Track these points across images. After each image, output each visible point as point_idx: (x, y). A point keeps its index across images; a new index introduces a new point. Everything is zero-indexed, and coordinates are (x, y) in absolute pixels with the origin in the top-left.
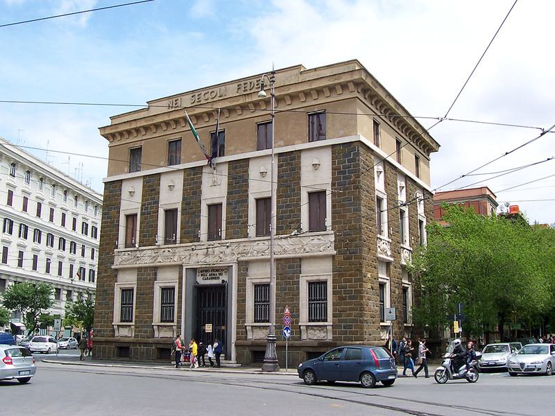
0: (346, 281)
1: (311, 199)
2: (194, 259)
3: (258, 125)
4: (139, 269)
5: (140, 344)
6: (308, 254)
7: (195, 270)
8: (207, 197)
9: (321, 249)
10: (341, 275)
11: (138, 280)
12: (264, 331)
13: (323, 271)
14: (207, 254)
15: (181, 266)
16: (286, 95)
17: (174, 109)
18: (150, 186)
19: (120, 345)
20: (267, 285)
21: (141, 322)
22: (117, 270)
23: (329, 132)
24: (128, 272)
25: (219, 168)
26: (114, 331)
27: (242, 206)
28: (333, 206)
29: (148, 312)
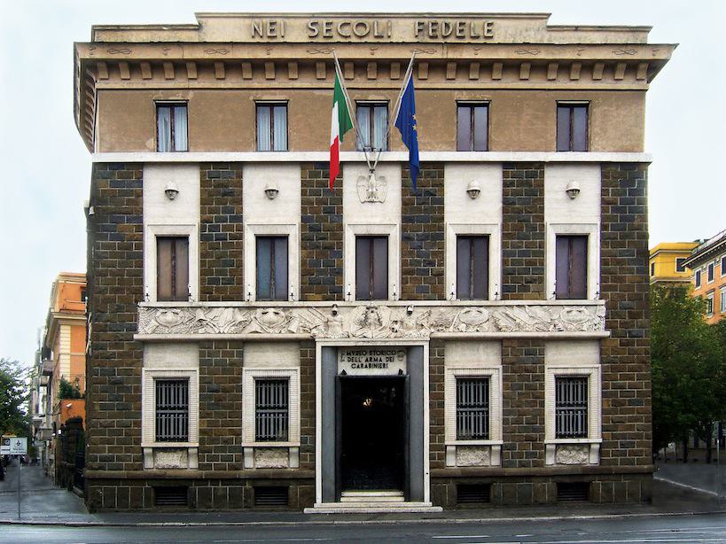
3: (158, 106)
5: (215, 480)
8: (355, 221)
11: (202, 363)
13: (585, 361)
14: (364, 323)
15: (311, 342)
17: (265, 40)
18: (219, 185)
20: (584, 380)
22: (145, 343)
23: (595, 140)
24: (268, 348)
26: (142, 458)
27: (433, 246)
28: (603, 262)
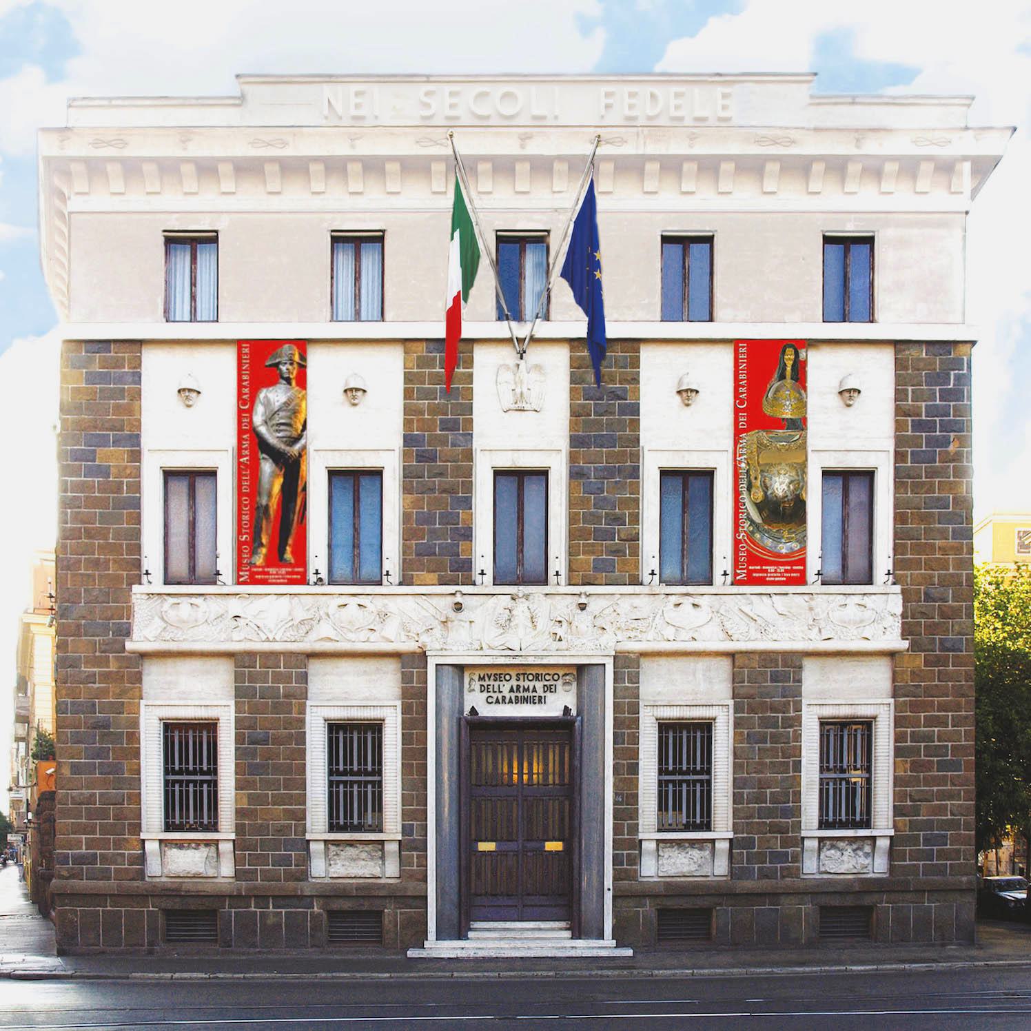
0: (931, 722)
1: (664, 487)
4: (732, 655)
5: (262, 899)
7: (460, 668)
12: (696, 853)
16: (272, 160)
19: (176, 904)
21: (261, 830)
22: (144, 655)
25: (536, 355)
28: (899, 518)
29: (289, 800)
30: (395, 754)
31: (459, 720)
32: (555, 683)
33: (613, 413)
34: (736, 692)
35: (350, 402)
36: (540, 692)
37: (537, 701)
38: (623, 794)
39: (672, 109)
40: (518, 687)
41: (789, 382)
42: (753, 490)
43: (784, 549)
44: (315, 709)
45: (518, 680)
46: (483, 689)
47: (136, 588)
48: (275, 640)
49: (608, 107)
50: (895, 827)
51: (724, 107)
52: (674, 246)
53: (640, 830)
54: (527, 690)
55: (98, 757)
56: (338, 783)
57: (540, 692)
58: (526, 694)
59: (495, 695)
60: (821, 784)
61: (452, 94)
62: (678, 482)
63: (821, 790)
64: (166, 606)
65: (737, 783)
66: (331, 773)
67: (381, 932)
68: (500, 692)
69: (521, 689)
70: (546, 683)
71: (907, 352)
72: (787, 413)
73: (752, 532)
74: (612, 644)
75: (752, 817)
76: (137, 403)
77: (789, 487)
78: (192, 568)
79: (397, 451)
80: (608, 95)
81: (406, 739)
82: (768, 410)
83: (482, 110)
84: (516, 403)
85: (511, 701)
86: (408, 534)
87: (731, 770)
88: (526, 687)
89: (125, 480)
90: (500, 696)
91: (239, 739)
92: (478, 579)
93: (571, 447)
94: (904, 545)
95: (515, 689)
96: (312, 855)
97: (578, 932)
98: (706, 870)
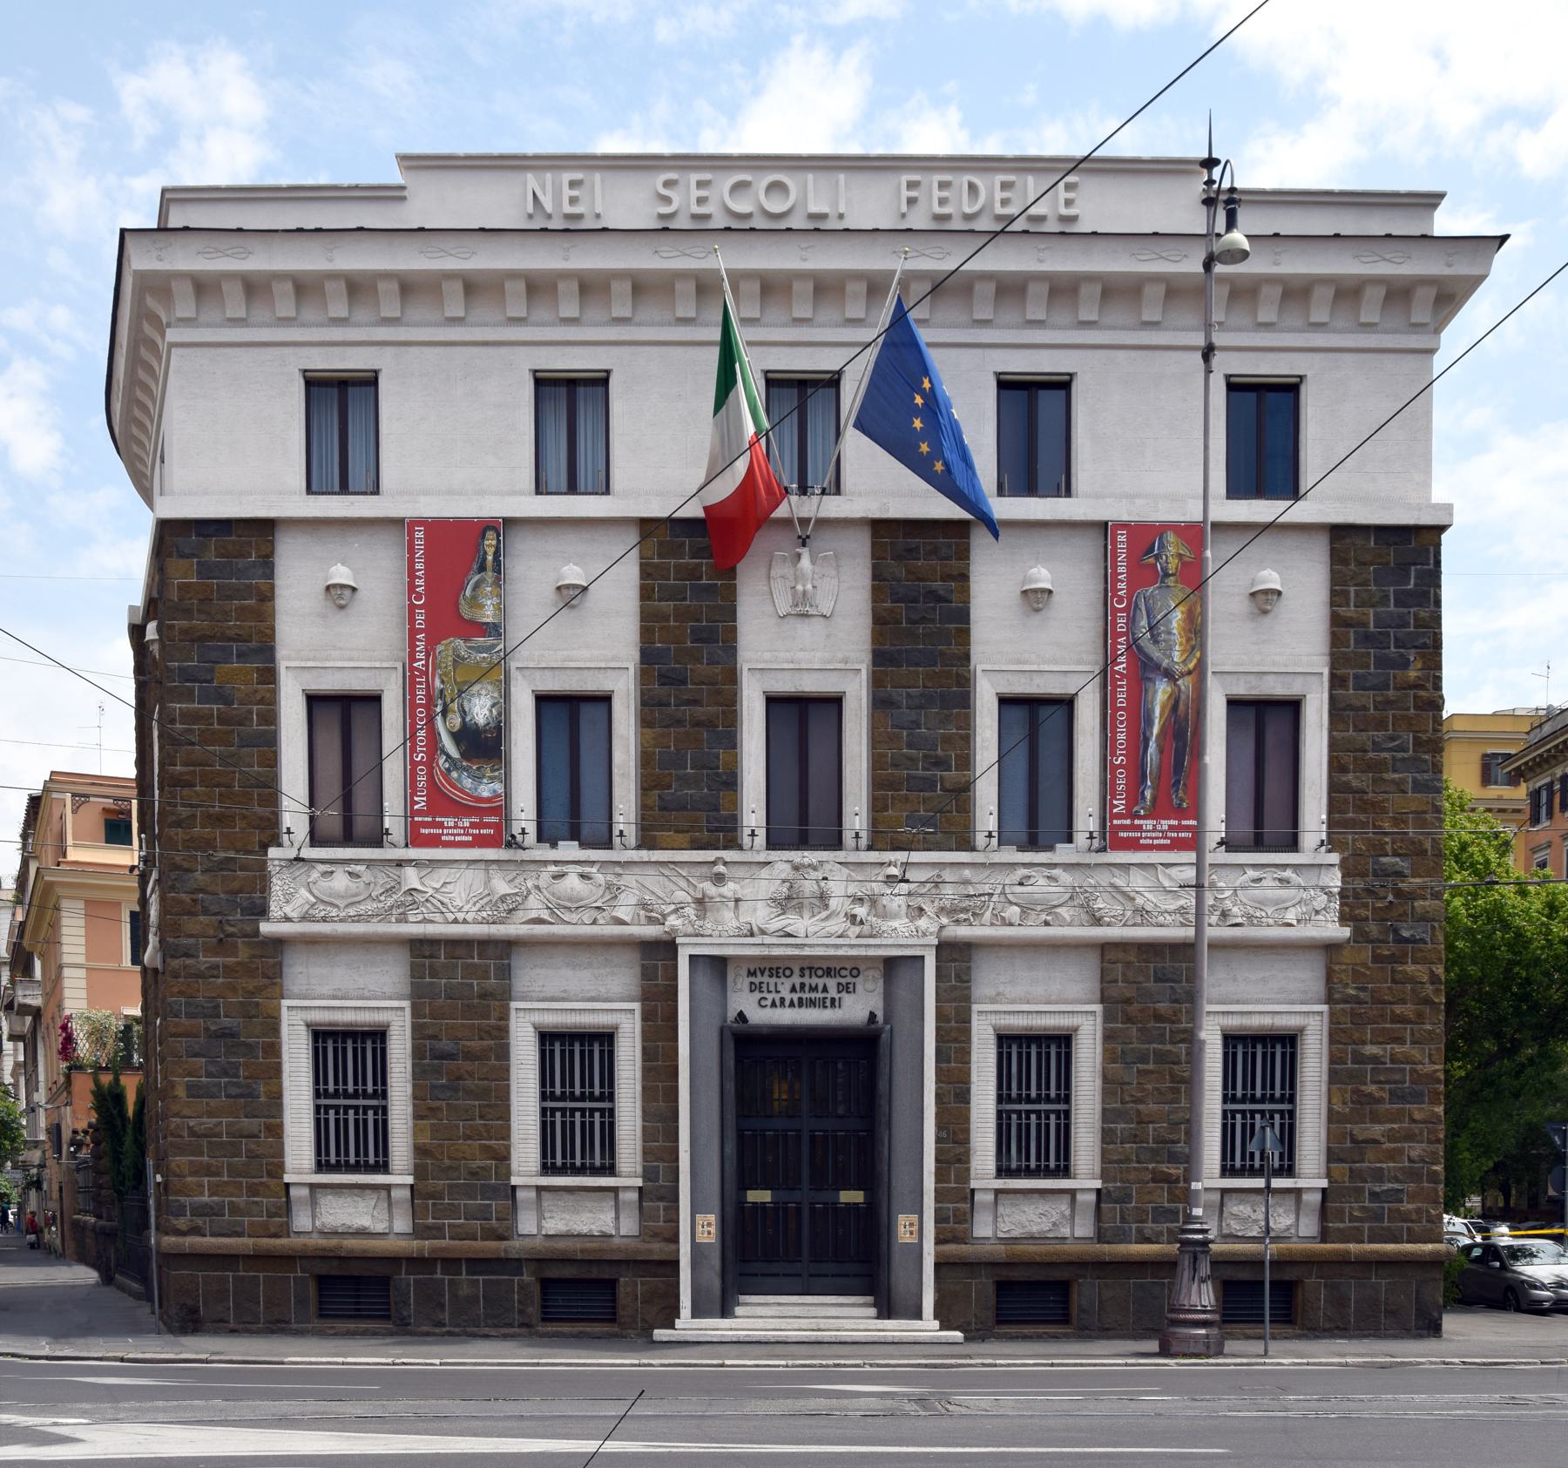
2: (729, 920)
5: (451, 1263)
6: (1237, 932)
9: (1291, 916)
10: (1358, 1020)
15: (665, 949)
19: (323, 1269)
30: (632, 1073)
31: (722, 1030)
32: (854, 980)
33: (933, 621)
34: (1106, 994)
35: (1031, 606)
36: (833, 993)
37: (828, 1004)
38: (948, 1129)
39: (998, 205)
40: (803, 985)
41: (489, 575)
42: (450, 716)
43: (485, 791)
44: (521, 1014)
45: (802, 976)
46: (753, 988)
47: (273, 852)
48: (465, 921)
49: (911, 201)
50: (1329, 1175)
51: (1068, 203)
52: (786, 392)
53: (972, 1177)
54: (814, 989)
55: (226, 1074)
56: (553, 1110)
57: (833, 993)
58: (813, 995)
59: (770, 997)
60: (1225, 1115)
61: (700, 184)
62: (1250, 714)
63: (1224, 1126)
64: (315, 875)
65: (1107, 1115)
66: (544, 1097)
67: (614, 1307)
68: (778, 992)
69: (807, 988)
70: (844, 981)
71: (1347, 541)
72: (488, 615)
73: (448, 770)
74: (934, 928)
75: (1128, 1160)
76: (269, 604)
77: (491, 711)
78: (348, 821)
79: (632, 671)
80: (912, 185)
81: (647, 1054)
82: (466, 612)
83: (742, 206)
84: (797, 605)
85: (792, 1004)
86: (649, 783)
87: (1098, 1098)
88: (813, 986)
89: (255, 707)
90: (777, 997)
91: (418, 1053)
92: (746, 841)
93: (874, 666)
94: (1346, 801)
95: (798, 988)
96: (519, 1204)
97: (886, 1310)
98: (1065, 1231)
